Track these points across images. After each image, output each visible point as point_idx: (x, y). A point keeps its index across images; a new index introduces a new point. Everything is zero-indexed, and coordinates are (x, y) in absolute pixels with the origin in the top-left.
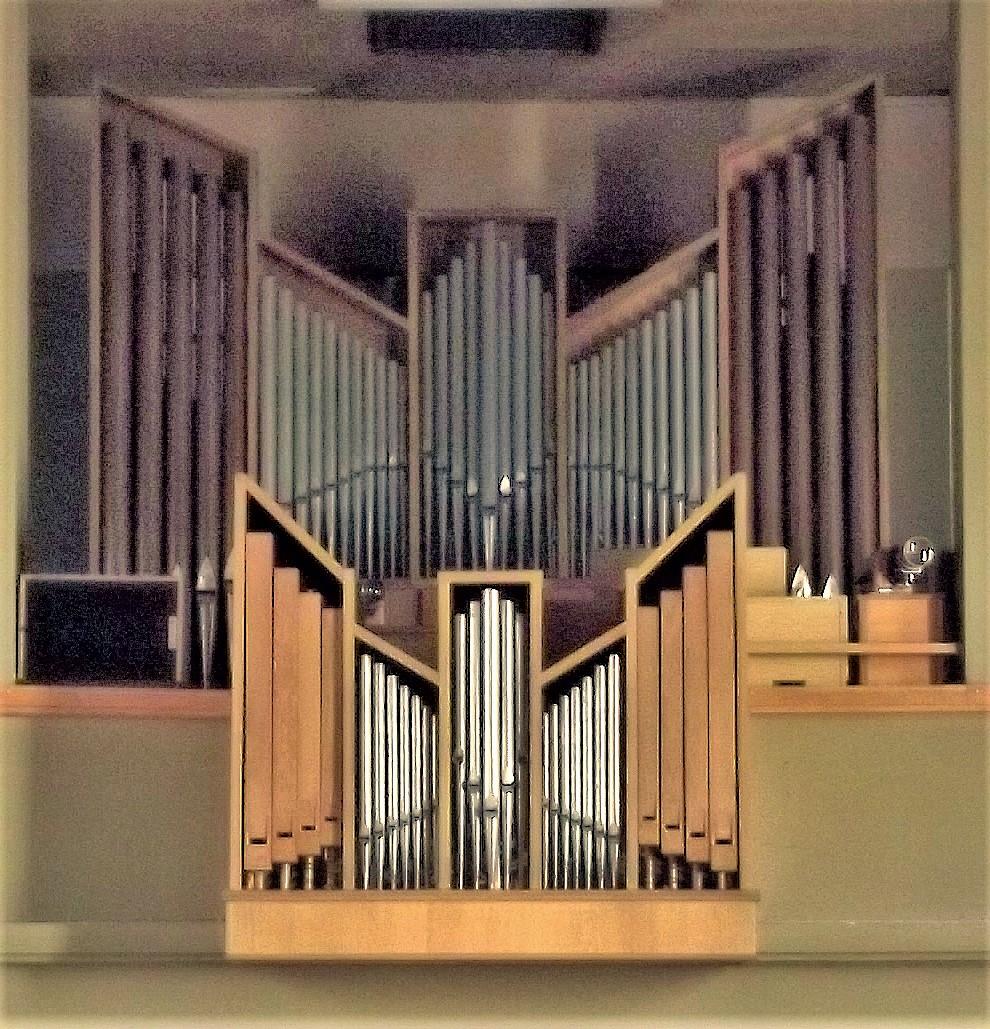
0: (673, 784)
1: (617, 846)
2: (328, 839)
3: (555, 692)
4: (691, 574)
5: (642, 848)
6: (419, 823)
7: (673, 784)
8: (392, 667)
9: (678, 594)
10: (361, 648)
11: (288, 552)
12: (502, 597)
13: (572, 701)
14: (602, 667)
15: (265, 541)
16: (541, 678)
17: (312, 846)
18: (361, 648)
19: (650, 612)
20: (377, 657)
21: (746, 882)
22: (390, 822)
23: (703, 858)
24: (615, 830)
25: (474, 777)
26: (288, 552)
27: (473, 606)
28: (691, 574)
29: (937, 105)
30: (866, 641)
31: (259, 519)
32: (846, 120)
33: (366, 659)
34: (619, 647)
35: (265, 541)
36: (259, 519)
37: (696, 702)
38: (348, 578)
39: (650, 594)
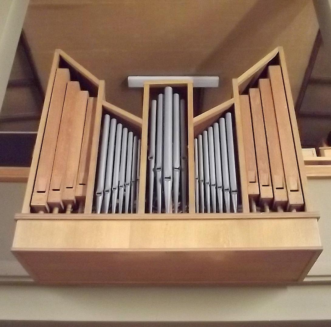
0: (263, 165)
1: (236, 195)
2: (79, 193)
3: (200, 131)
4: (263, 82)
5: (250, 196)
6: (129, 187)
7: (263, 165)
8: (120, 120)
9: (257, 89)
10: (105, 111)
11: (75, 76)
12: (174, 92)
13: (210, 134)
14: (223, 119)
15: (66, 72)
16: (194, 121)
17: (71, 196)
18: (105, 111)
19: (246, 97)
20: (113, 115)
21: (308, 207)
22: (106, 189)
23: (285, 199)
24: (234, 187)
25: (159, 165)
26: (75, 76)
27: (161, 96)
28: (263, 82)
29: (247, 96)
30: (322, 247)
31: (63, 64)
32: (172, 88)
33: (108, 117)
34: (232, 109)
35: (66, 72)
36: (63, 64)
37: (271, 131)
38: (101, 85)
39: (245, 91)
